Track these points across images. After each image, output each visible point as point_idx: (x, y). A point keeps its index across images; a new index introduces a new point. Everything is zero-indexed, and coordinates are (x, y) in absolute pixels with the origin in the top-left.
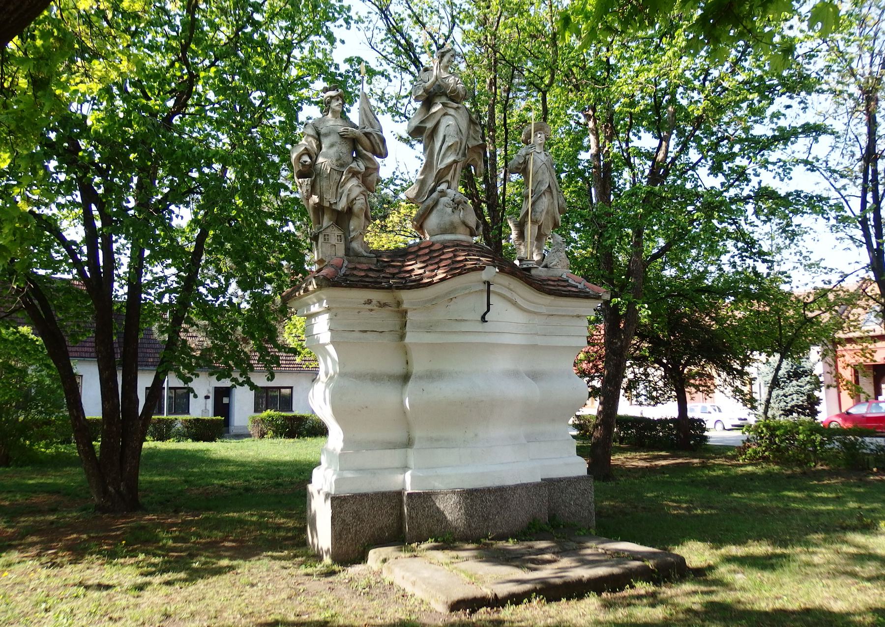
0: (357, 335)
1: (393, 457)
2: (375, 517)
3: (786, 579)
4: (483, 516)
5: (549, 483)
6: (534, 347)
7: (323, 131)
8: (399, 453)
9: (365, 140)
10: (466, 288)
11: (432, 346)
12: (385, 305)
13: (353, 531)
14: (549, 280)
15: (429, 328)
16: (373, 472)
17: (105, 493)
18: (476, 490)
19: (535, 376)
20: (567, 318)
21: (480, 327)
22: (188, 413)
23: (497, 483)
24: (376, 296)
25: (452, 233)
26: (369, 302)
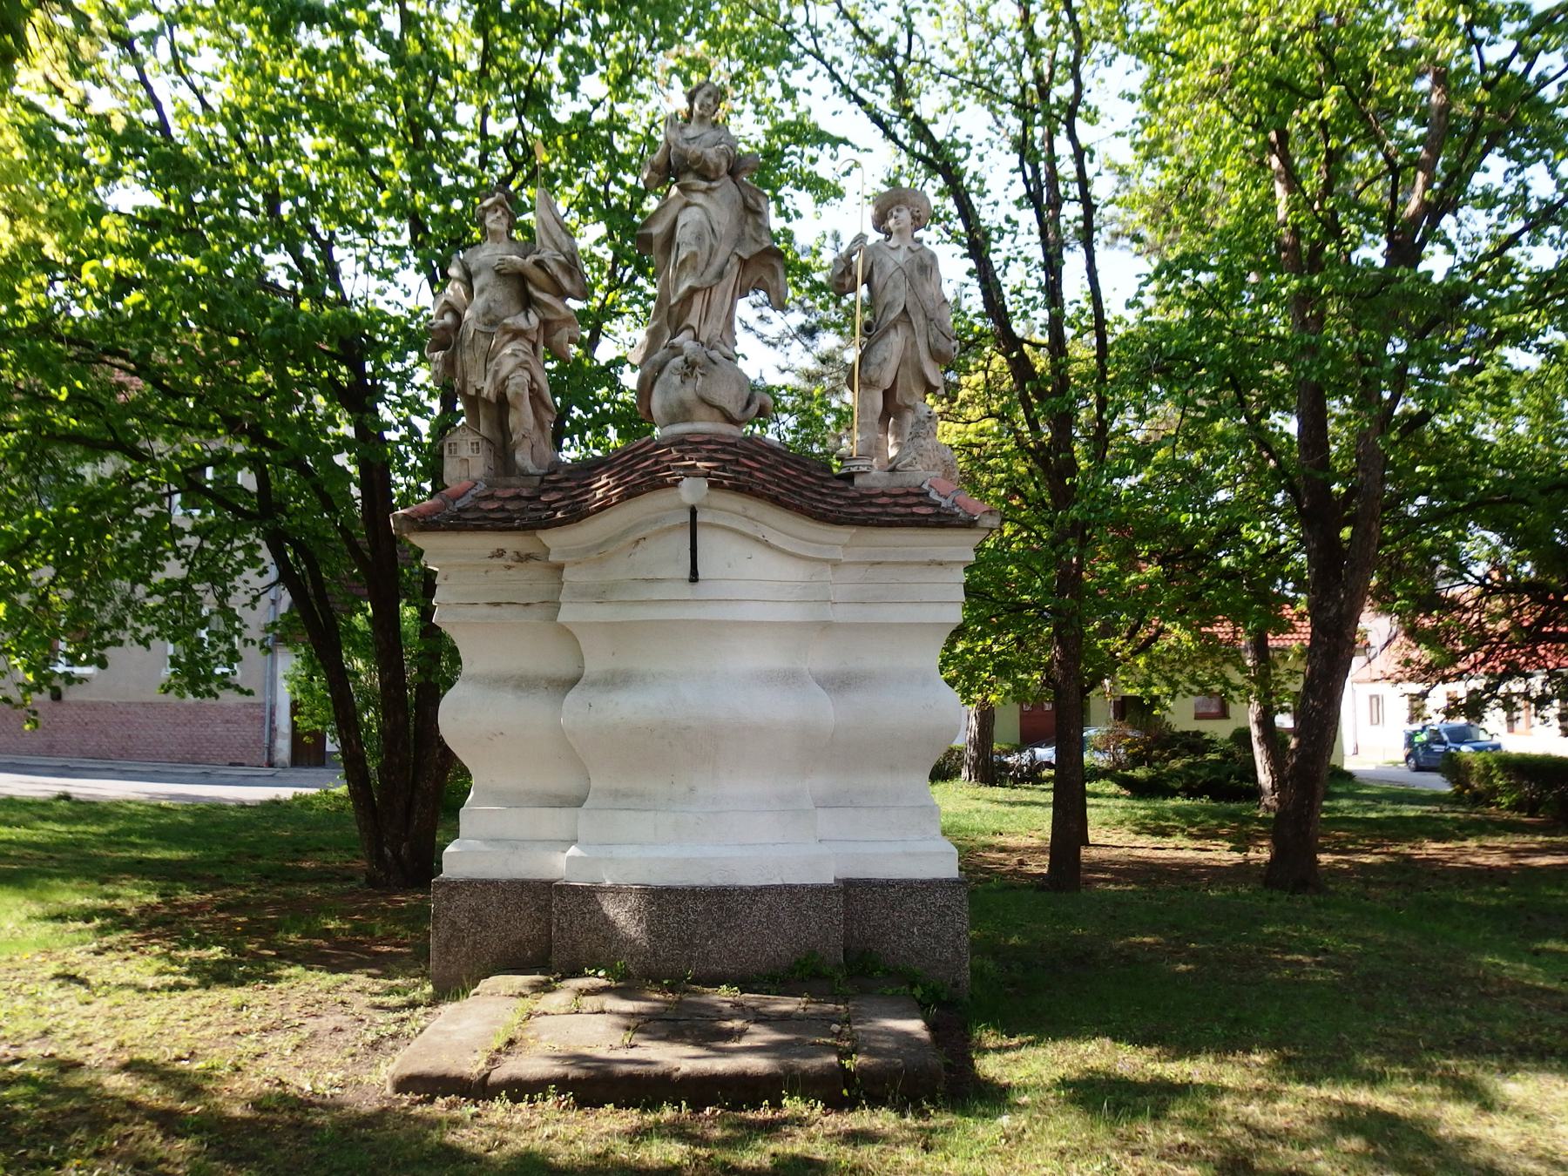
0: (486, 610)
1: (553, 821)
2: (508, 922)
3: (1542, 1143)
4: (681, 939)
5: (851, 889)
6: (826, 626)
7: (473, 268)
8: (564, 814)
9: (536, 274)
10: (656, 521)
11: (610, 626)
12: (528, 557)
13: (469, 942)
14: (908, 494)
15: (601, 596)
16: (516, 844)
17: (378, 857)
18: (669, 890)
19: (838, 683)
20: (916, 567)
21: (687, 591)
23: (717, 880)
24: (512, 542)
26: (500, 553)
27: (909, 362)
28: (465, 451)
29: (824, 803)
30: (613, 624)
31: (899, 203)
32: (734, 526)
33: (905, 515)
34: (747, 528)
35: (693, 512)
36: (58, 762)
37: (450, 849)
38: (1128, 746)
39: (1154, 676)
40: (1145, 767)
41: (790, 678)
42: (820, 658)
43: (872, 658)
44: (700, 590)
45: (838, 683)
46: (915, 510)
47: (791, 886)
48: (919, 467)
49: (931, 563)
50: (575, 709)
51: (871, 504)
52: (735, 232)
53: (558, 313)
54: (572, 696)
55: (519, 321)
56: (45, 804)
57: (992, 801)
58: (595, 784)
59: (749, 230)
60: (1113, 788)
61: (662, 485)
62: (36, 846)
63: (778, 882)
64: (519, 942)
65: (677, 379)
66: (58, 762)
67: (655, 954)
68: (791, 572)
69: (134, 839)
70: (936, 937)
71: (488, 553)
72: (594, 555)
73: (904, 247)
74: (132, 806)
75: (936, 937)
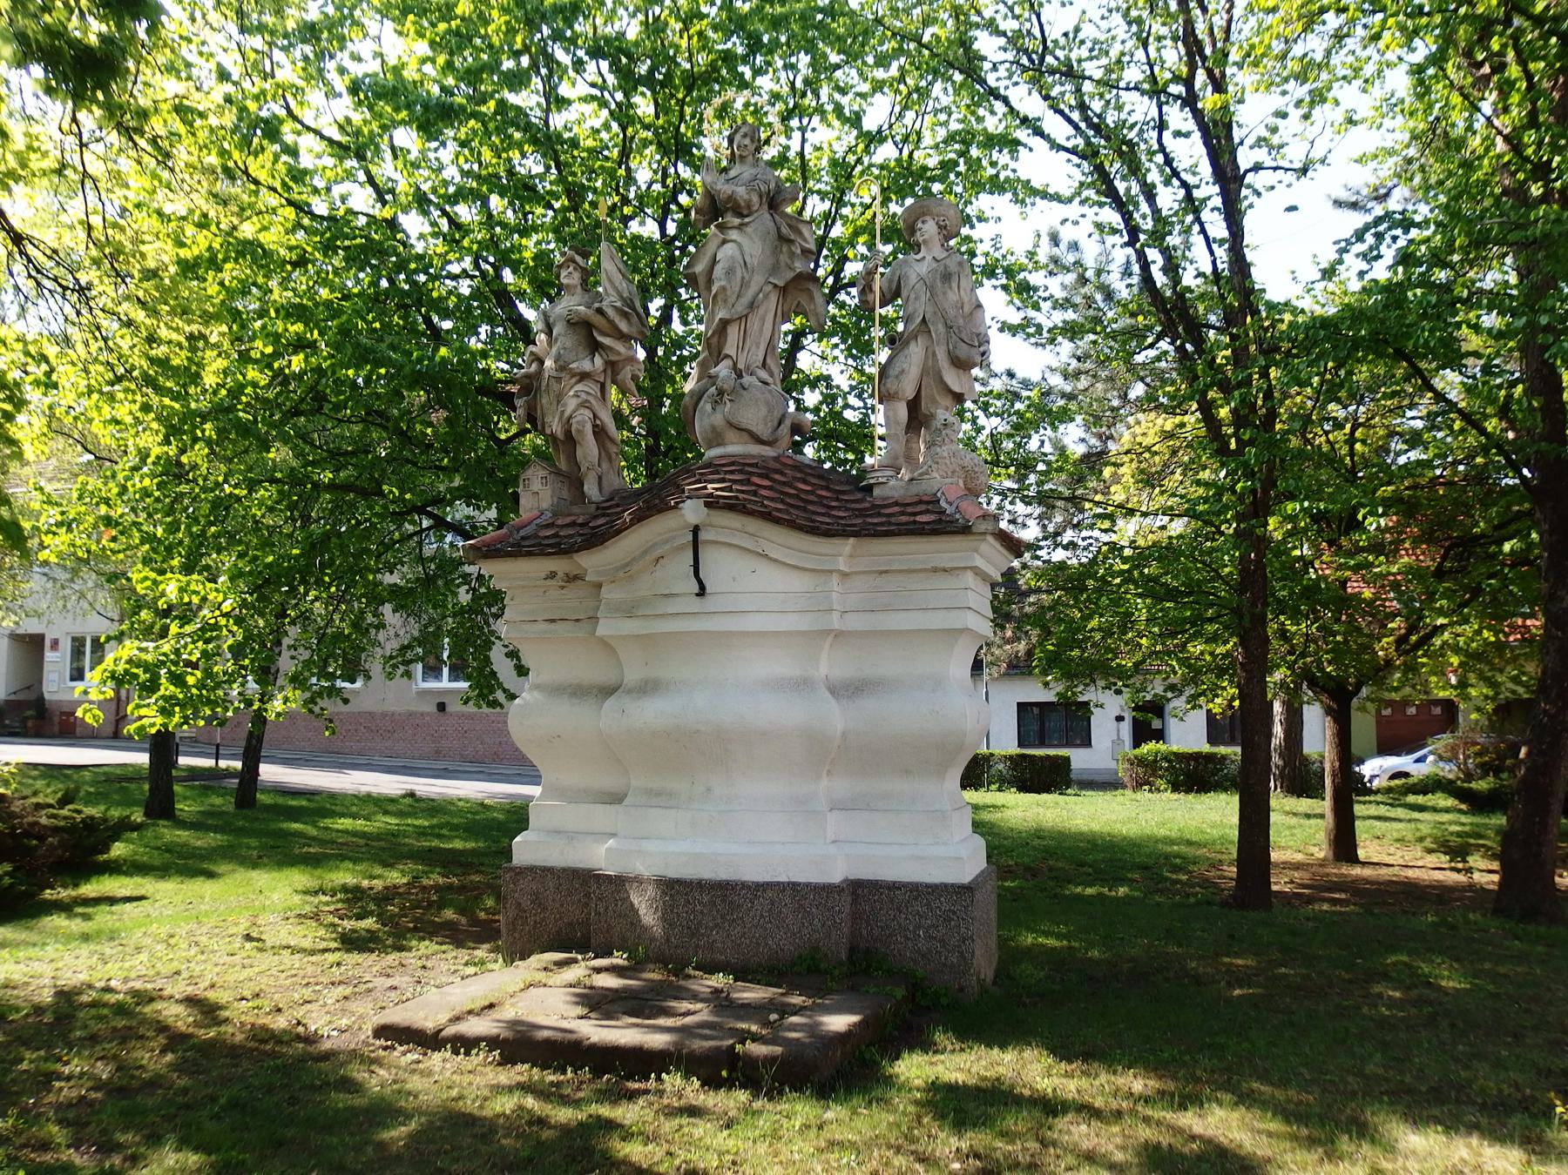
1: (603, 816)
5: (858, 889)
9: (597, 320)
10: (666, 542)
12: (576, 578)
14: (921, 502)
15: (629, 610)
16: (570, 835)
18: (679, 882)
19: (849, 690)
21: (696, 605)
22: (1023, 708)
23: (723, 874)
25: (719, 445)
26: (553, 575)
27: (930, 371)
28: (536, 485)
29: (838, 806)
30: (638, 637)
31: (924, 214)
32: (735, 542)
33: (906, 523)
34: (747, 543)
35: (696, 530)
36: (440, 765)
37: (518, 839)
38: (1478, 754)
39: (1472, 675)
40: (1491, 779)
41: (802, 685)
42: (829, 665)
43: (887, 664)
44: (709, 603)
45: (849, 690)
46: (918, 518)
47: (794, 884)
48: (935, 475)
49: (935, 570)
50: (611, 715)
51: (879, 515)
52: (770, 262)
53: (619, 353)
54: (610, 702)
55: (586, 365)
56: (392, 800)
57: (1287, 813)
58: (634, 783)
59: (784, 258)
60: (1451, 802)
61: (664, 508)
62: (363, 835)
63: (783, 879)
64: (571, 924)
65: (709, 407)
66: (440, 765)
67: (668, 940)
68: (797, 583)
69: (444, 831)
70: (942, 941)
71: (543, 575)
72: (621, 574)
73: (929, 258)
74: (461, 804)
75: (942, 941)
